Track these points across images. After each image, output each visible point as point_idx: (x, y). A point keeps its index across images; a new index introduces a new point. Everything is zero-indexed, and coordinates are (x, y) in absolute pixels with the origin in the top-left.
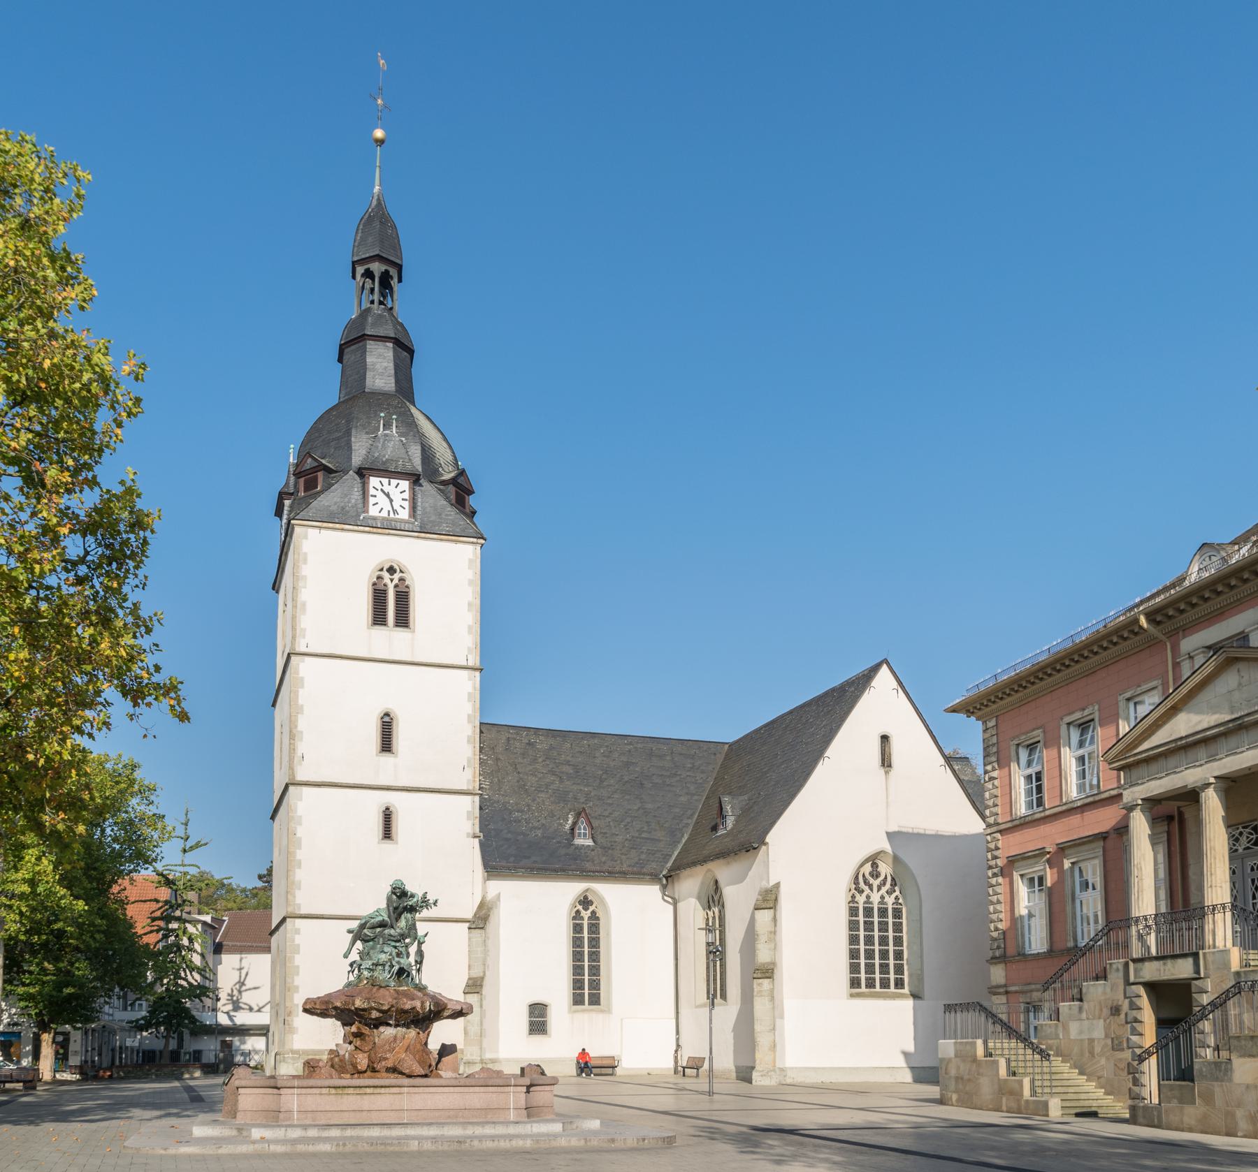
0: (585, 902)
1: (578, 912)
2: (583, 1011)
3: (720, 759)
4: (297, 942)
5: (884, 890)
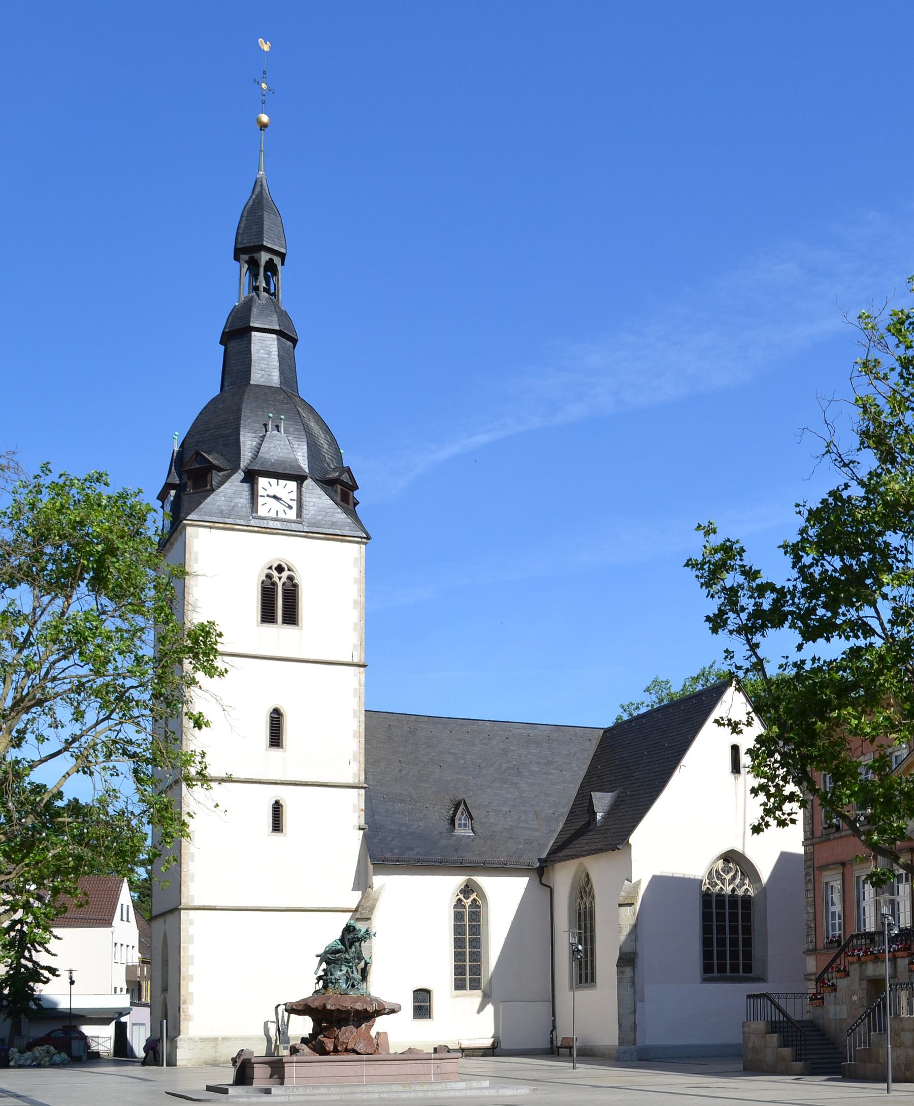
0: (468, 889)
1: (460, 900)
2: (464, 996)
3: (591, 748)
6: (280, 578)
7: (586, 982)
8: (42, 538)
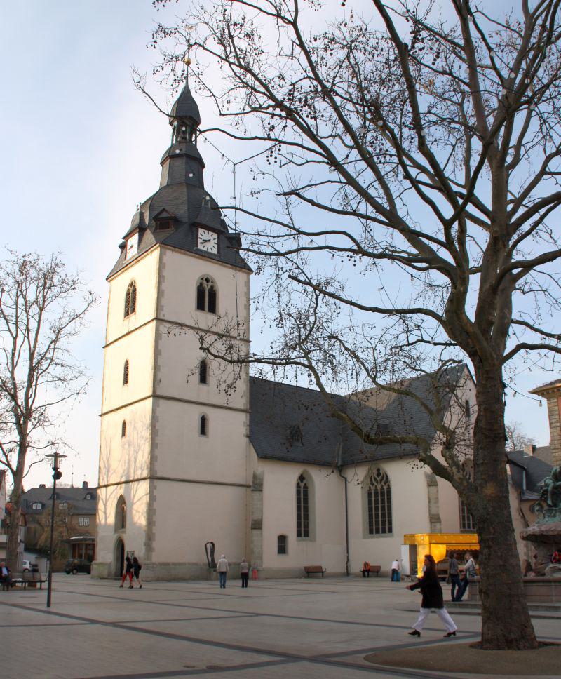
0: (301, 478)
5: (383, 483)
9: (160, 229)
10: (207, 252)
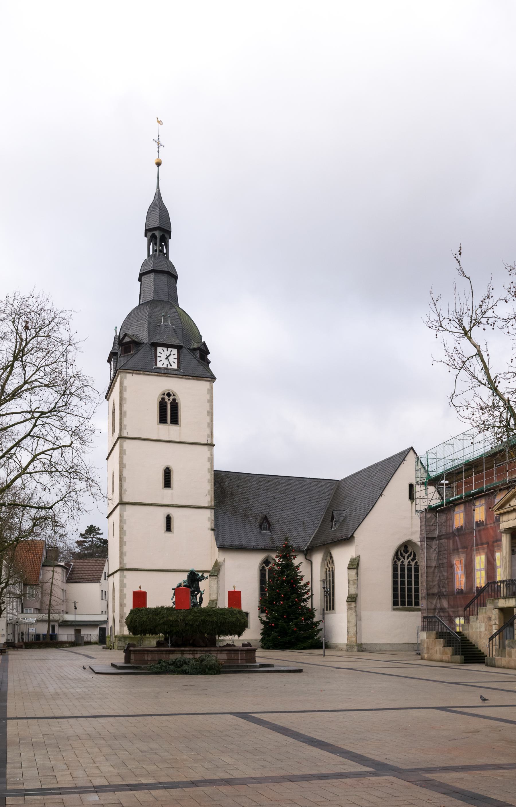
1: (263, 567)
4: (125, 582)
5: (410, 559)
6: (169, 400)
7: (330, 609)
8: (186, 663)
9: (124, 354)
10: (166, 369)
